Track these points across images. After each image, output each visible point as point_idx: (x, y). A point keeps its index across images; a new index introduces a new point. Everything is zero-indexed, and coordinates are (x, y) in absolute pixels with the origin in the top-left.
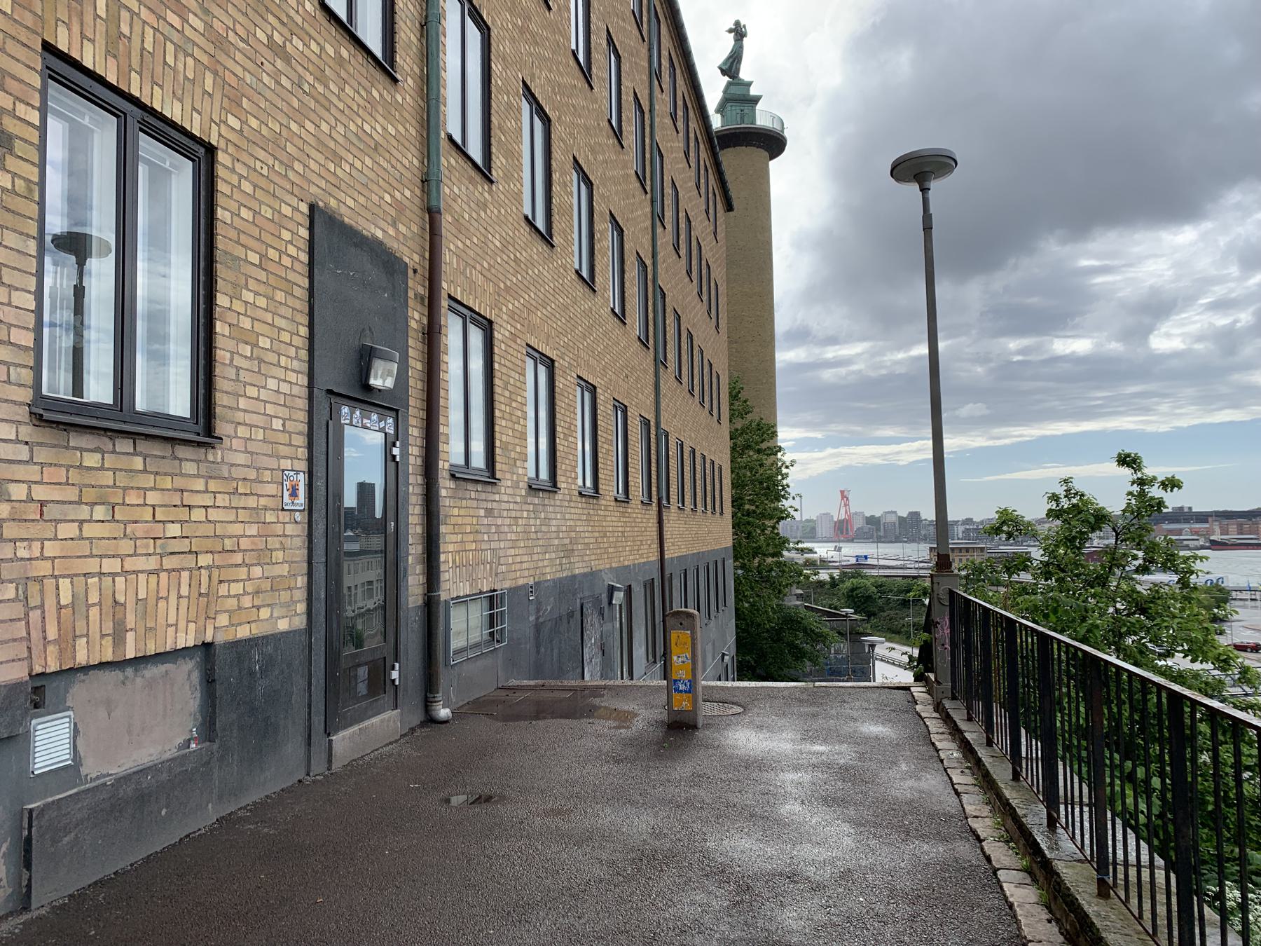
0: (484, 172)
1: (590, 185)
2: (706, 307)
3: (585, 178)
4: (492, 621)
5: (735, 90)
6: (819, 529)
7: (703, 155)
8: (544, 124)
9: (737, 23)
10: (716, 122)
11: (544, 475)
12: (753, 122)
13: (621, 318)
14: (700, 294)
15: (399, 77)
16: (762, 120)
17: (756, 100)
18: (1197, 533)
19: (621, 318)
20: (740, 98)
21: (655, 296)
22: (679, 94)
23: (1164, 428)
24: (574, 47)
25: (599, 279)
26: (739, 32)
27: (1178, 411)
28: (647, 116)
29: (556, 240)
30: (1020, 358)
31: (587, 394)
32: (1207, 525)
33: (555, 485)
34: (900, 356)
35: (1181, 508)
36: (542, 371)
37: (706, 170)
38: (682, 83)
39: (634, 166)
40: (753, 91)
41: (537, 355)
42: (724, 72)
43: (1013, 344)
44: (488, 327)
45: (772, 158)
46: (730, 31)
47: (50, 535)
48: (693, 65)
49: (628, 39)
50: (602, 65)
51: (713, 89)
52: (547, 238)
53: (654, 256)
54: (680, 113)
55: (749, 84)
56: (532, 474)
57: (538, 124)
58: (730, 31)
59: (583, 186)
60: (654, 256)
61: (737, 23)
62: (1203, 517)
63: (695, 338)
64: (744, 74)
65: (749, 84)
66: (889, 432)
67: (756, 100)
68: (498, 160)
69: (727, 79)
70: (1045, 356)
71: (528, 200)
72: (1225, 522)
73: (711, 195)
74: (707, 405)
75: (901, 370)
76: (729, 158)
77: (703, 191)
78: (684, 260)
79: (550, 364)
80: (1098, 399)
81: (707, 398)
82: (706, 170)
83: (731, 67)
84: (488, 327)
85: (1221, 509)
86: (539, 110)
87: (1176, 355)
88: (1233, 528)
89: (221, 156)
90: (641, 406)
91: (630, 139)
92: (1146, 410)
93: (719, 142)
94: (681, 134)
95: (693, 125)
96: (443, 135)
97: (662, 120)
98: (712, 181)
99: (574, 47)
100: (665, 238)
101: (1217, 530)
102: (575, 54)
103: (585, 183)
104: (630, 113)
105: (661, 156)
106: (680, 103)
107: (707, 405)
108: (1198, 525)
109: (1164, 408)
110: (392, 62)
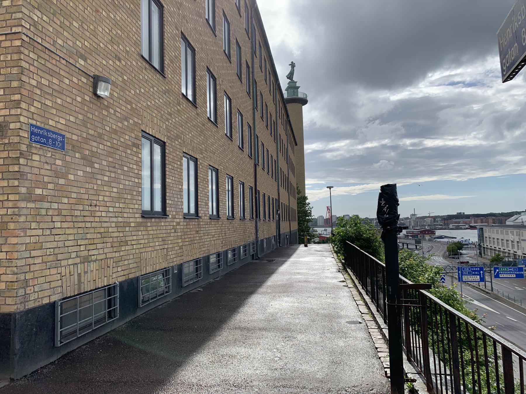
1: (215, 79)
2: (265, 124)
3: (188, 45)
4: (197, 270)
5: (292, 85)
6: (318, 222)
7: (281, 105)
8: (192, 52)
9: (292, 62)
10: (285, 96)
11: (215, 213)
12: (298, 96)
13: (242, 149)
14: (267, 126)
15: (166, 76)
16: (300, 96)
17: (298, 87)
18: (466, 223)
19: (242, 149)
20: (293, 87)
21: (254, 137)
23: (465, 179)
24: (207, 17)
25: (234, 137)
26: (293, 65)
27: (472, 172)
28: (251, 70)
29: (168, 71)
30: (411, 148)
31: (214, 173)
32: (469, 220)
33: (219, 217)
34: (360, 147)
35: (461, 213)
36: (192, 164)
40: (297, 85)
41: (189, 157)
42: (288, 78)
43: (408, 142)
46: (290, 65)
47: (28, 245)
48: (264, 31)
50: (222, 29)
51: (284, 83)
52: (215, 123)
53: (254, 123)
55: (296, 82)
56: (211, 213)
57: (189, 52)
58: (290, 65)
59: (211, 80)
60: (254, 123)
61: (292, 62)
62: (468, 216)
63: (265, 146)
65: (296, 82)
66: (352, 181)
67: (298, 87)
68: (219, 120)
69: (289, 80)
70: (421, 148)
72: (476, 219)
73: (263, 61)
74: (266, 170)
75: (358, 153)
76: (289, 106)
77: (263, 69)
79: (217, 171)
80: (441, 166)
81: (274, 175)
82: (270, 73)
83: (290, 76)
84: (196, 161)
85: (486, 213)
86: (188, 45)
87: (476, 147)
88: (479, 221)
89: (167, 144)
90: (250, 182)
91: (234, 59)
92: (459, 171)
93: (285, 102)
95: (288, 128)
97: (257, 69)
98: (272, 79)
99: (207, 17)
100: (258, 115)
101: (473, 222)
102: (207, 21)
104: (234, 46)
105: (256, 83)
107: (266, 170)
108: (466, 220)
109: (467, 171)
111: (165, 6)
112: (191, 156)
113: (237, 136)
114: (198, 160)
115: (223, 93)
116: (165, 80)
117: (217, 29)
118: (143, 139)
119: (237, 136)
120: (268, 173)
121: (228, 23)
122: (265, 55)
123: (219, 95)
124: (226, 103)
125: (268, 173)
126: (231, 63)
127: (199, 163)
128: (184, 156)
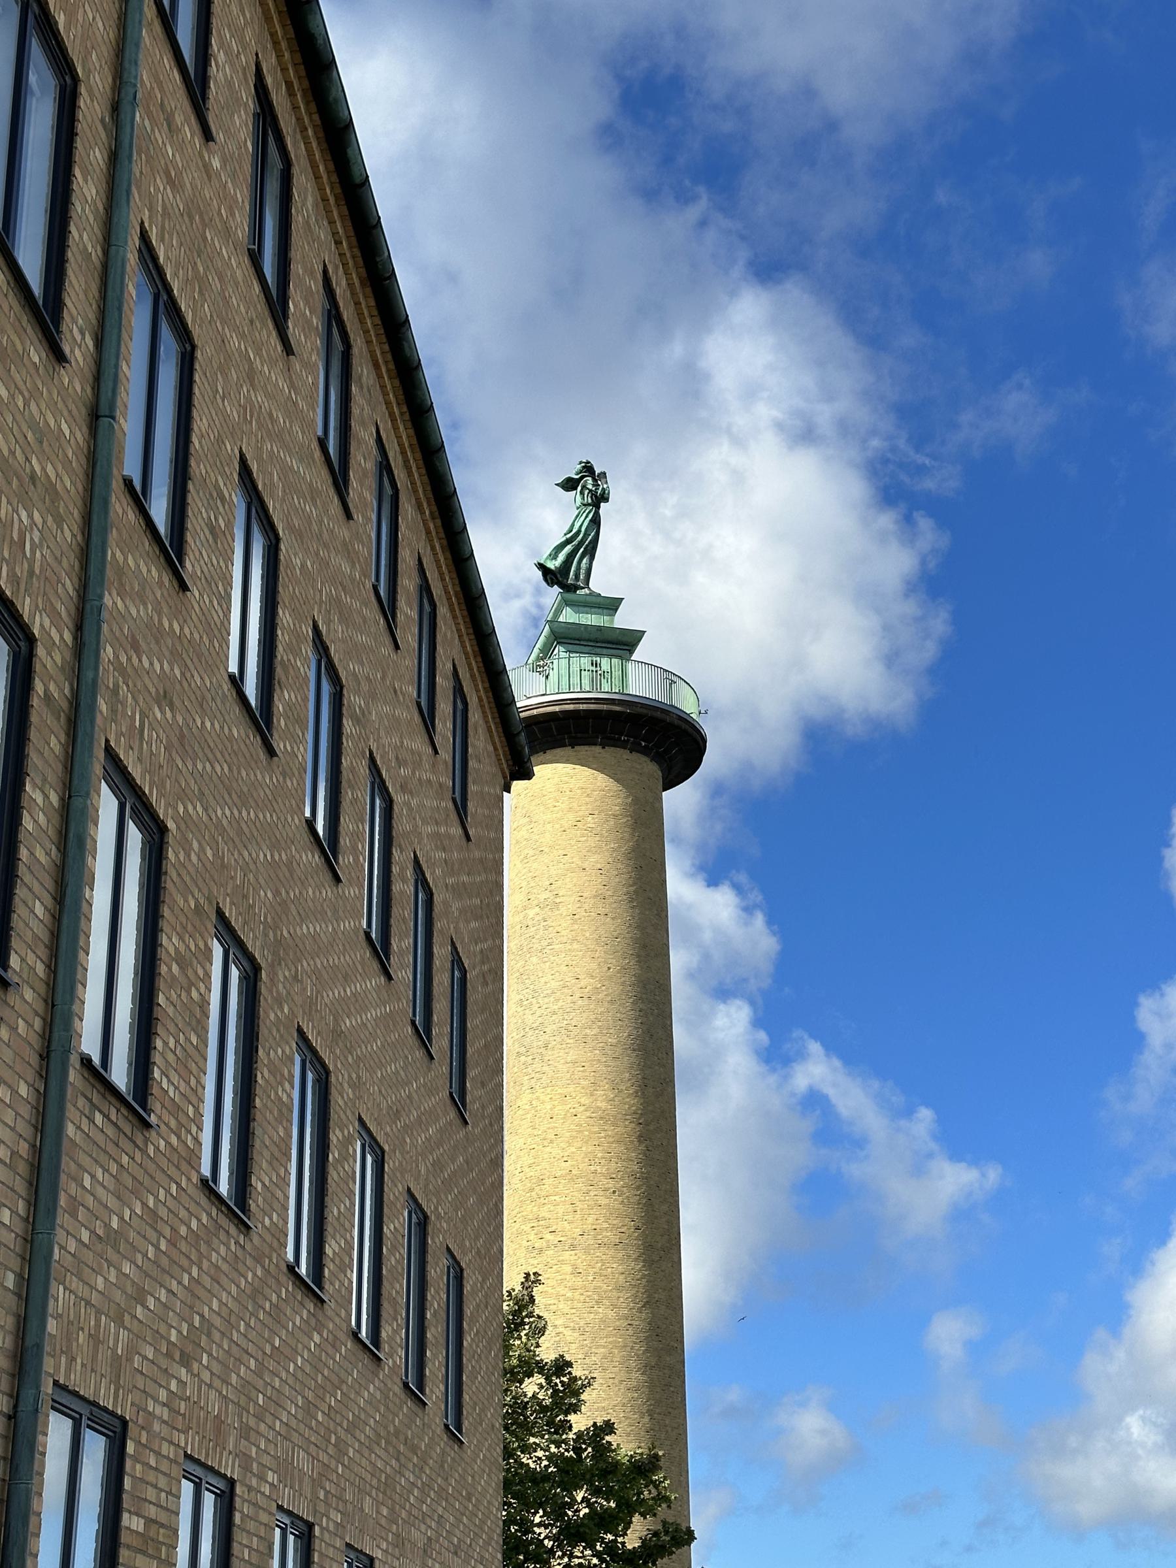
0: (137, 1104)
2: (402, 1003)
15: (153, 1119)
22: (406, 558)
31: (209, 1500)
36: (95, 1448)
37: (458, 690)
38: (482, 730)
39: (364, 920)
41: (85, 1410)
44: (118, 1435)
45: (669, 784)
46: (569, 485)
48: (348, 126)
49: (358, 640)
54: (444, 707)
63: (340, 1080)
64: (601, 582)
71: (211, 1147)
78: (441, 1068)
84: (118, 1435)
94: (445, 755)
96: (74, 1060)
102: (237, 682)
103: (141, 826)
106: (408, 583)
107: (435, 1392)
110: (244, 1208)
111: (171, 825)
112: (95, 1404)
113: (352, 1280)
114: (132, 1429)
115: (353, 1127)
116: (322, 1308)
117: (280, 722)
118: (183, 1480)
119: (352, 1280)
120: (415, 1391)
121: (184, 334)
122: (329, 254)
123: (335, 1136)
124: (218, 980)
125: (415, 1391)
126: (337, 879)
127: (130, 1448)
128: (184, 1477)
